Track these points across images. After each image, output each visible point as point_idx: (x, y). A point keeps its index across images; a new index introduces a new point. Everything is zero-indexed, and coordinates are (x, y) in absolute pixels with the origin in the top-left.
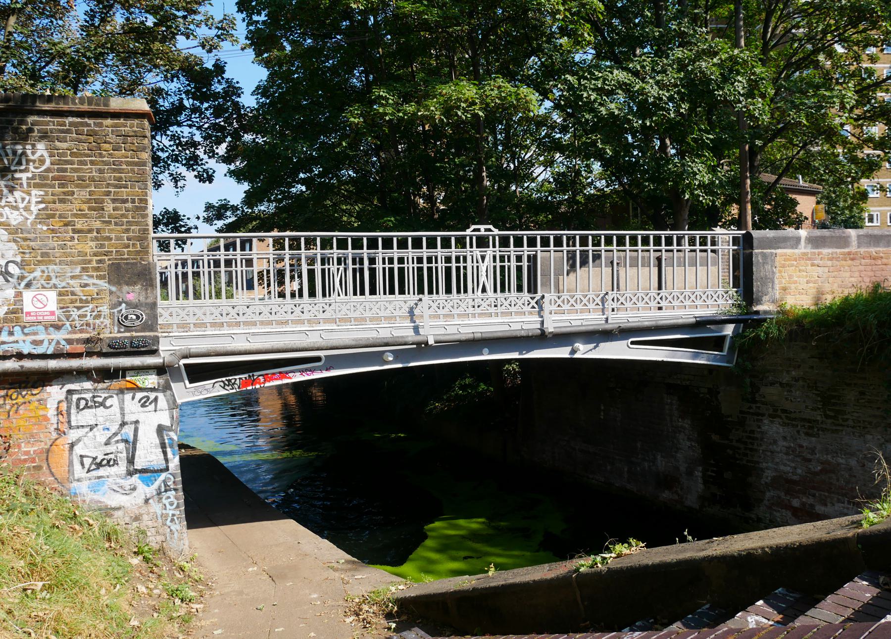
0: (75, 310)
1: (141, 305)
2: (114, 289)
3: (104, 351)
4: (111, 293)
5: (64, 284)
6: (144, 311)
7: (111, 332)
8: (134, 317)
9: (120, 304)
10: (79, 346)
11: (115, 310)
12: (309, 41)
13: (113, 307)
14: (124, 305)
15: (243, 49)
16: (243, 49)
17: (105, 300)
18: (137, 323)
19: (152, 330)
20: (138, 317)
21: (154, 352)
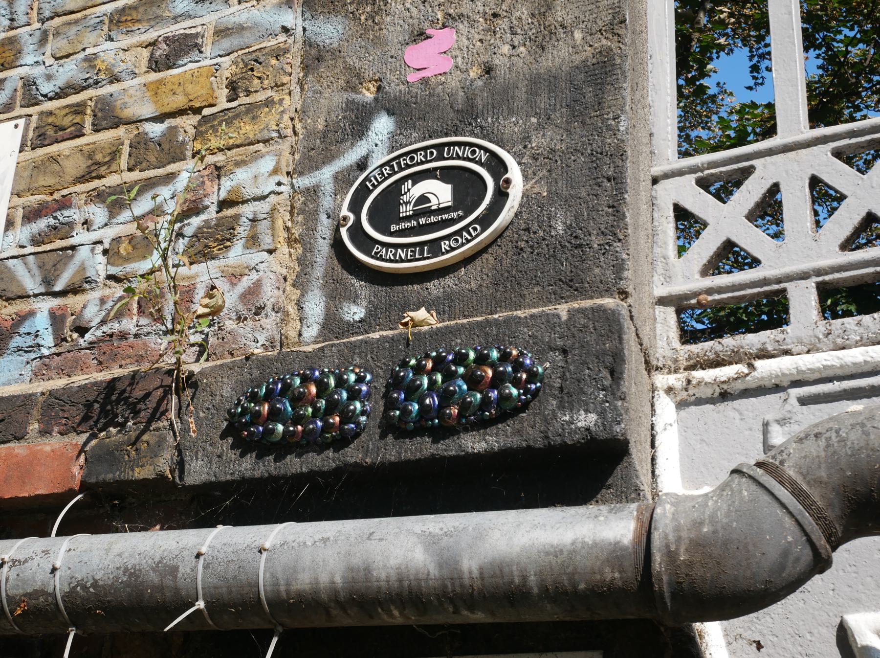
0: (98, 213)
1: (503, 100)
2: (330, 30)
3: (198, 472)
4: (315, 57)
5: (69, 71)
6: (520, 145)
7: (268, 303)
8: (441, 193)
9: (358, 122)
10: (54, 443)
11: (326, 175)
12: (705, 530)
13: (318, 150)
14: (382, 125)
15: (731, 94)
16: (731, 94)
17: (269, 119)
18: (460, 241)
19: (573, 286)
20: (467, 187)
21: (592, 468)
